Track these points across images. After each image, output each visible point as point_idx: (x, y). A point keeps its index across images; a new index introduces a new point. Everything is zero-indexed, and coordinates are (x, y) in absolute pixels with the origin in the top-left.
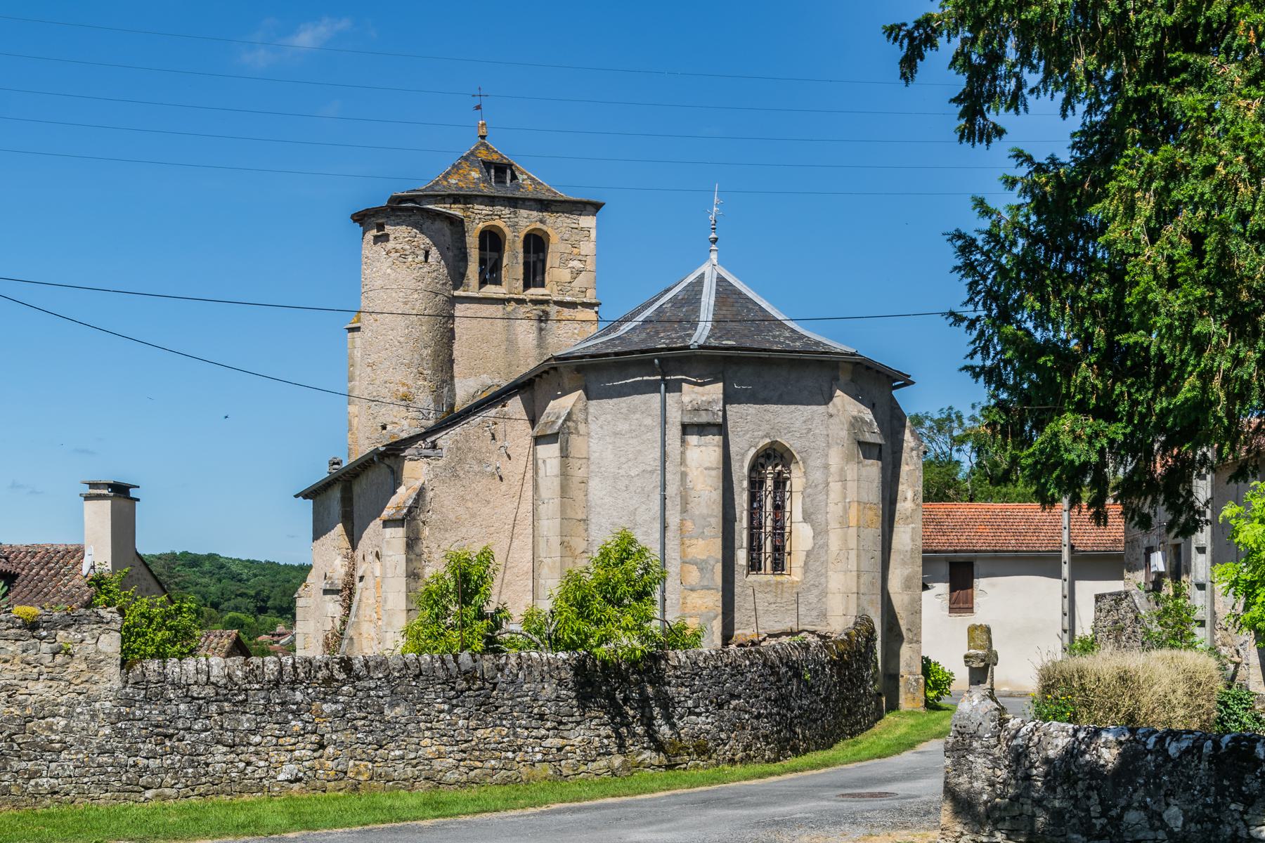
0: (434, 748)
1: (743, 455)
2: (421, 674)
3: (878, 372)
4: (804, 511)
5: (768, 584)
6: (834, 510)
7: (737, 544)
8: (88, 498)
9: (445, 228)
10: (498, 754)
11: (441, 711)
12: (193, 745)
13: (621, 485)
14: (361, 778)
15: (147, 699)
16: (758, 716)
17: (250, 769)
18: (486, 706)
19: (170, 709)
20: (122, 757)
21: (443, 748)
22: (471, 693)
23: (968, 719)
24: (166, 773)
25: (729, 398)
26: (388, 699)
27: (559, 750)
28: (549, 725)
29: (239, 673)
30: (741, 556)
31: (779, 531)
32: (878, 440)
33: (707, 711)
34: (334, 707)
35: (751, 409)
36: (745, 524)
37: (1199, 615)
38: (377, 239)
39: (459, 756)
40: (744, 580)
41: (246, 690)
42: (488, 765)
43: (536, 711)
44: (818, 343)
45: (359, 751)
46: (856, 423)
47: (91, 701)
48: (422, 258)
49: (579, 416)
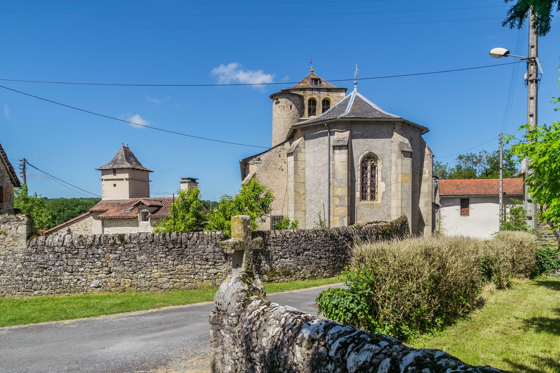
0: (158, 273)
1: (358, 157)
2: (153, 241)
3: (414, 126)
4: (382, 177)
5: (368, 204)
6: (393, 177)
7: (356, 190)
8: (182, 183)
9: (297, 98)
10: (187, 276)
11: (162, 257)
12: (55, 272)
13: (316, 170)
14: (126, 286)
15: (37, 253)
16: (321, 258)
17: (79, 282)
18: (182, 255)
19: (46, 257)
20: (26, 277)
21: (162, 273)
22: (175, 249)
23: (223, 298)
24: (44, 283)
25: (352, 137)
26: (138, 252)
27: (215, 274)
28: (210, 263)
29: (76, 241)
30: (358, 194)
31: (373, 185)
32: (410, 150)
33: (290, 256)
34: (115, 256)
35: (361, 141)
36: (359, 182)
37: (528, 214)
38: (276, 103)
39: (169, 277)
40: (358, 202)
41: (78, 249)
42: (182, 281)
43: (204, 257)
44: (388, 116)
45: (126, 274)
46: (401, 144)
47: (14, 253)
48: (289, 108)
49: (301, 146)
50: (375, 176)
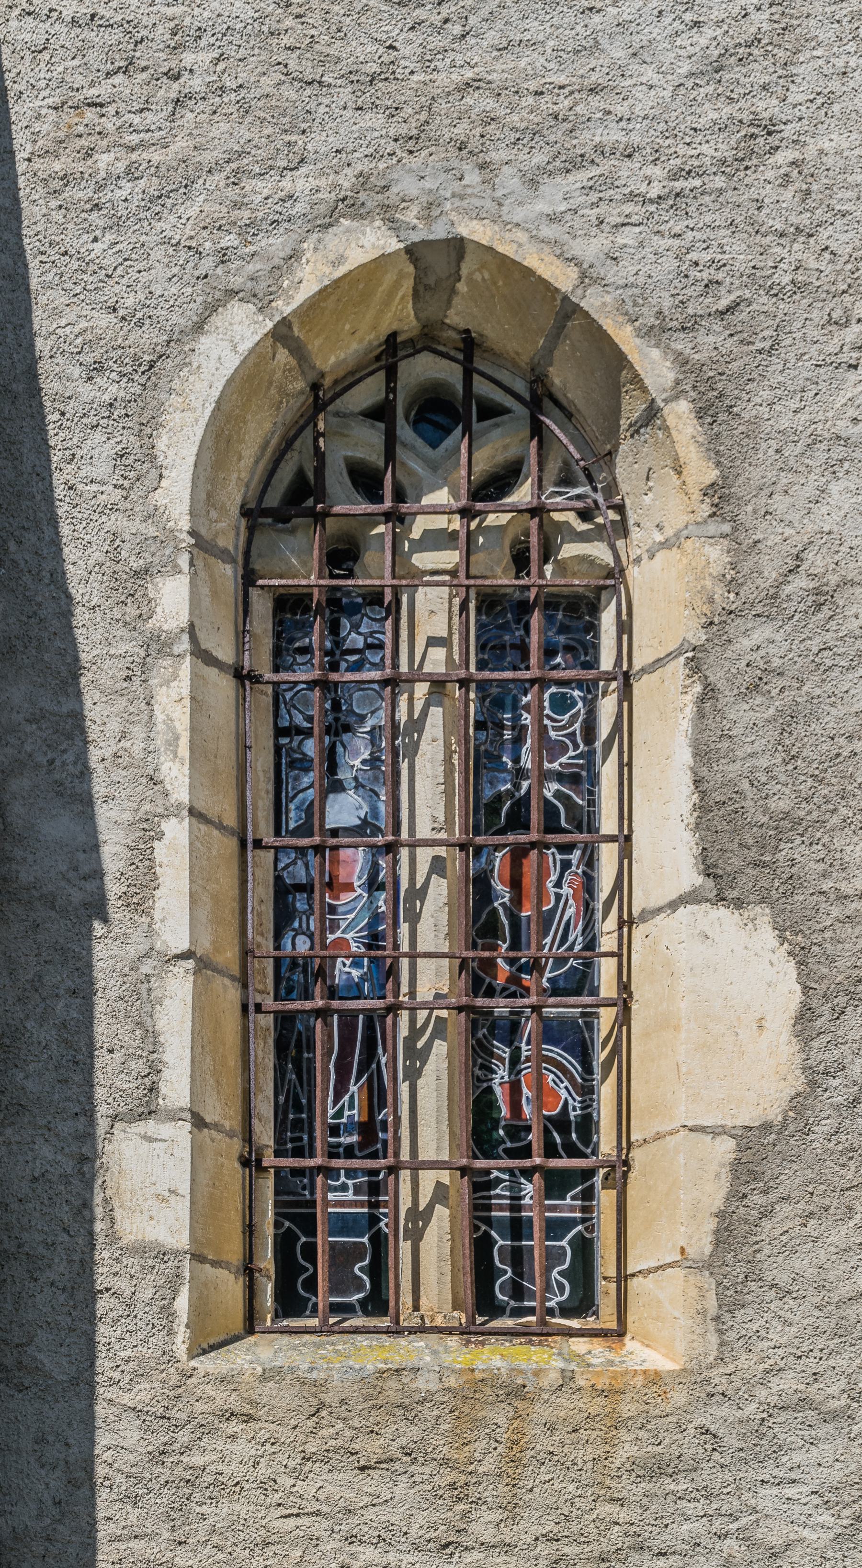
4: (713, 809)
5: (390, 1399)
36: (173, 920)
50: (585, 820)
